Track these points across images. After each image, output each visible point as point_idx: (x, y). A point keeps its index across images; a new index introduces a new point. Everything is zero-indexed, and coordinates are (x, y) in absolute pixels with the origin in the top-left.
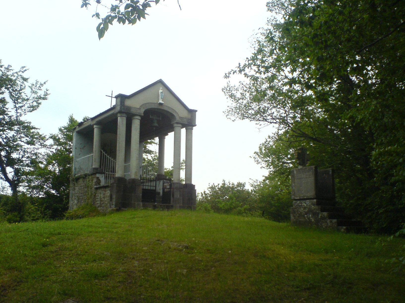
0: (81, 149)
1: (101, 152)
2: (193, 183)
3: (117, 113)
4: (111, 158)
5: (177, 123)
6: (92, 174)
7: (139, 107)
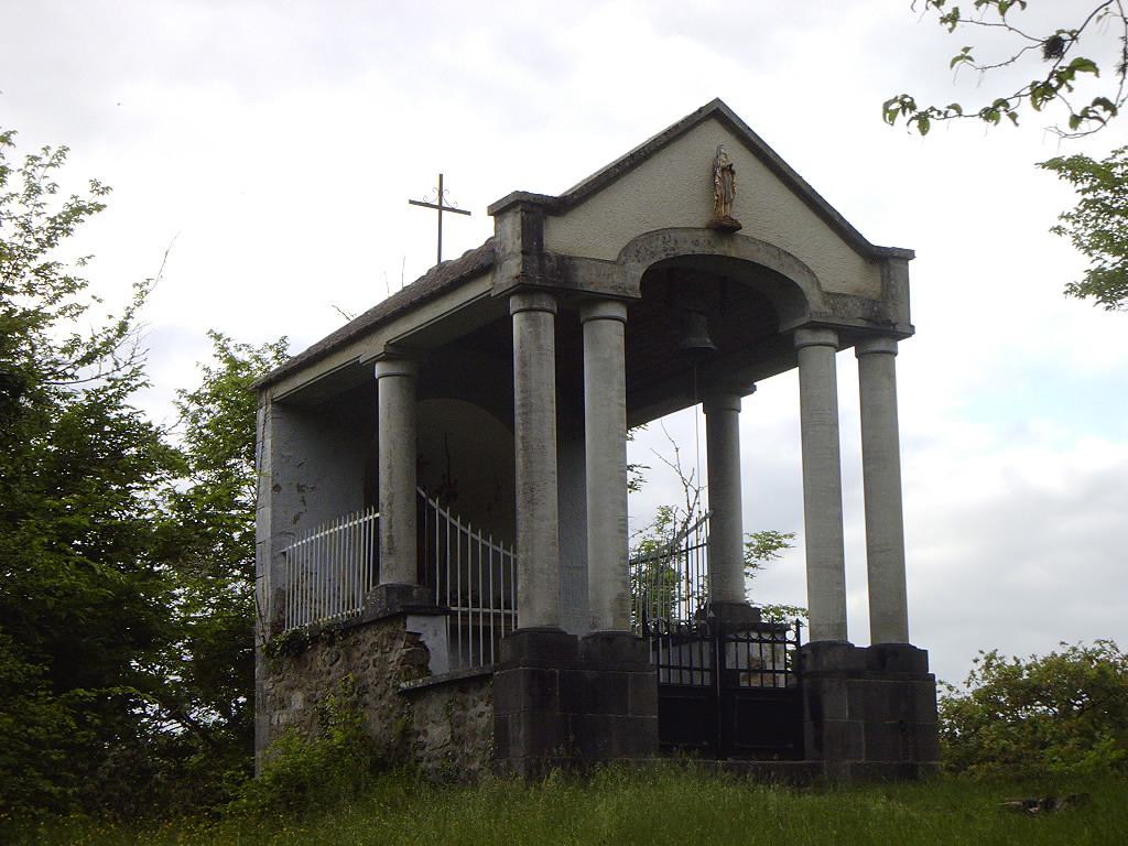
0: (300, 488)
1: (420, 501)
2: (915, 641)
3: (505, 297)
4: (490, 544)
5: (815, 327)
6: (377, 622)
7: (613, 256)
